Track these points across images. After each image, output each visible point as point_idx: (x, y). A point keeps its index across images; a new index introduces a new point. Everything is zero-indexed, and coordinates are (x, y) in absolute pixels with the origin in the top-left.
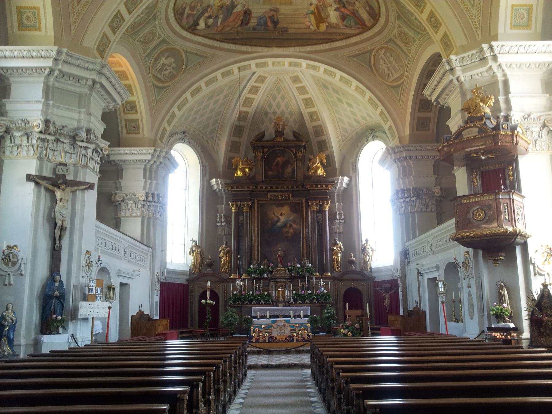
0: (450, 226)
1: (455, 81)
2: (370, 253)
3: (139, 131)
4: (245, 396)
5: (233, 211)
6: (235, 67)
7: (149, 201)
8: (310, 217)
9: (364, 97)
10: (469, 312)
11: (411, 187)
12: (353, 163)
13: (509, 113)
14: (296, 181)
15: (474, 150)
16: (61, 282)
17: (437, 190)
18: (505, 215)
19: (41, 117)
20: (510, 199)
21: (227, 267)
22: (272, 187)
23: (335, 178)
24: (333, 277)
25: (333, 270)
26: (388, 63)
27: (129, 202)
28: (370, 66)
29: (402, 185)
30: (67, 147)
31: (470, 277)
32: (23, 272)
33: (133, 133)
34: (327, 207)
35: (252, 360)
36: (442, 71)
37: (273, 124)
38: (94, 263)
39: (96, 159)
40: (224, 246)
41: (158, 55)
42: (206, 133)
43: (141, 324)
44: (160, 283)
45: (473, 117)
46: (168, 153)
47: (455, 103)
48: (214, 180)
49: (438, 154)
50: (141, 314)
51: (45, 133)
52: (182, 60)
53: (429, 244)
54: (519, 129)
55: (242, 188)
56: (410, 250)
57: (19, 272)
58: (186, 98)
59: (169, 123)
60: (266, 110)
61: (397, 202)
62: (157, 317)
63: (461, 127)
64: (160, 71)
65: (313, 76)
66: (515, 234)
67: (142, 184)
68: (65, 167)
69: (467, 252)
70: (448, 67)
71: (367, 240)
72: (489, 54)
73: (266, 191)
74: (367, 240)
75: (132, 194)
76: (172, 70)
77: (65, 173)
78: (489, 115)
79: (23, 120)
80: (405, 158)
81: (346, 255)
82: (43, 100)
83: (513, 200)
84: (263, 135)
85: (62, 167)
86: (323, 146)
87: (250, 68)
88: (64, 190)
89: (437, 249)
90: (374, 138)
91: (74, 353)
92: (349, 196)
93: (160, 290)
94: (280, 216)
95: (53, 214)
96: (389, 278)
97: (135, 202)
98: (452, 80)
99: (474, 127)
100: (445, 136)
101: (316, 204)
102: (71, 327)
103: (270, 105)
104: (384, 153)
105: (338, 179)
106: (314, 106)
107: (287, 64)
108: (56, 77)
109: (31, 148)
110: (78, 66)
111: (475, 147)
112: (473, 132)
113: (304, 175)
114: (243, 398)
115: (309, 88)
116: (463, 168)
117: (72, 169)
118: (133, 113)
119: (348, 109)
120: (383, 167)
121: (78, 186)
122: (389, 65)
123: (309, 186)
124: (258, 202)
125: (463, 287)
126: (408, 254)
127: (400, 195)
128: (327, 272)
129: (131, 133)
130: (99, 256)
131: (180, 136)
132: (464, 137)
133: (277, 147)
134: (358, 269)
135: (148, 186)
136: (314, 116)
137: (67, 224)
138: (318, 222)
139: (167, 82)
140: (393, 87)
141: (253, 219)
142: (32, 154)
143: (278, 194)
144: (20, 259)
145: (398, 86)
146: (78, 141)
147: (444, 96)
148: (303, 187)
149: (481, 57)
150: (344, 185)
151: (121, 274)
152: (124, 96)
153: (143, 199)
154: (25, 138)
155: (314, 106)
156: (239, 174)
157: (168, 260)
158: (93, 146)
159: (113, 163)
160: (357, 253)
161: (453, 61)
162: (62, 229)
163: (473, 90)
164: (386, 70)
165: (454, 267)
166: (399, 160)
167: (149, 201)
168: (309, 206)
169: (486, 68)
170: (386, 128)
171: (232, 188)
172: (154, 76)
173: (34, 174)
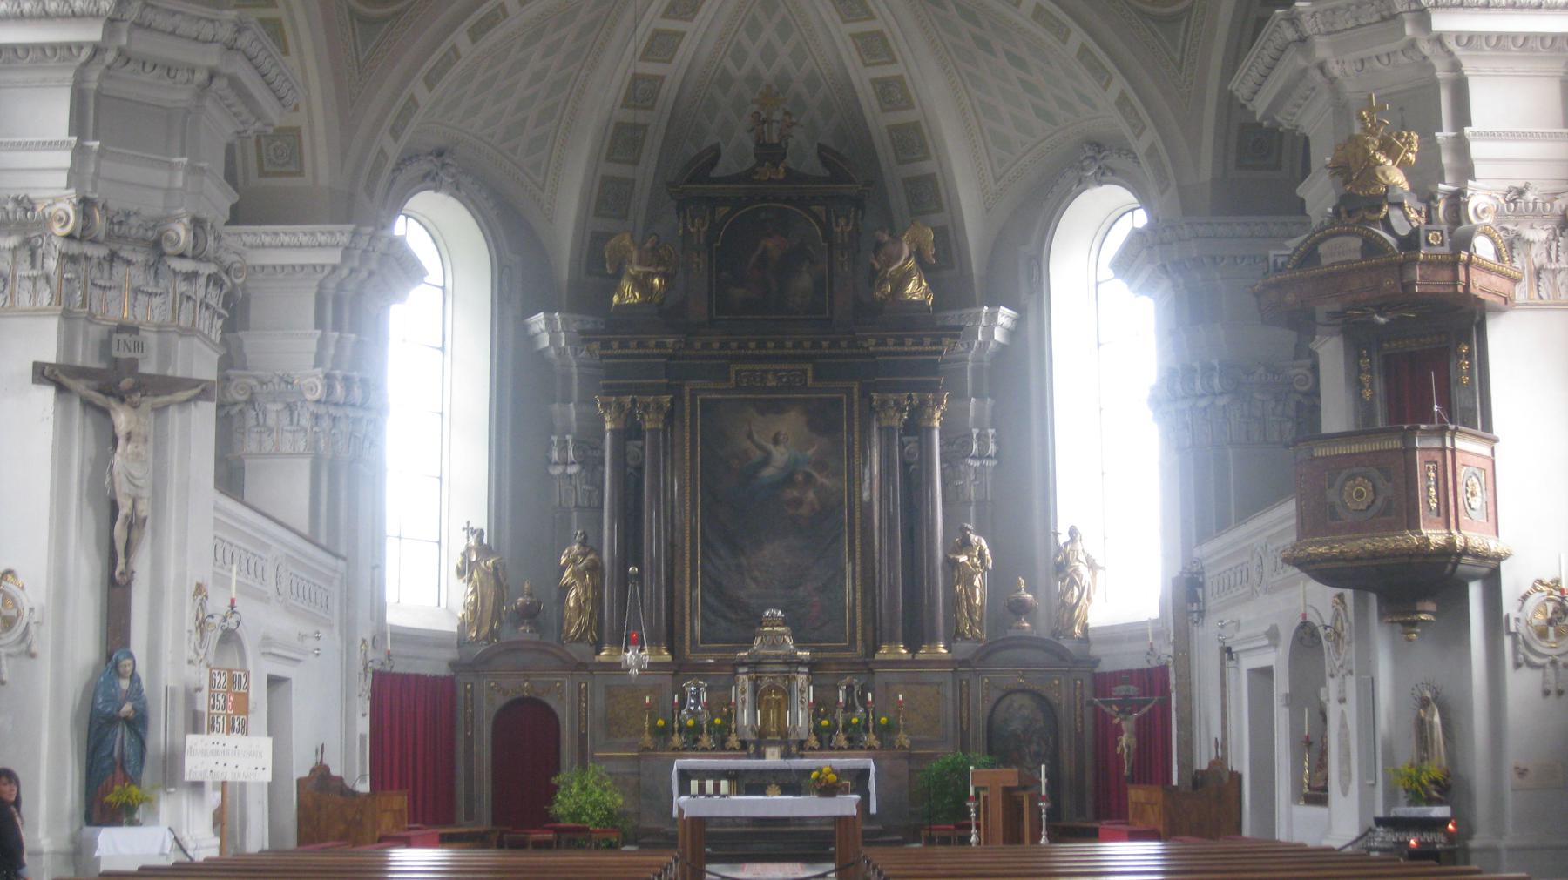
1: (1316, 75)
5: (608, 426)
16: (134, 677)
20: (1444, 449)
23: (966, 311)
24: (953, 661)
25: (954, 635)
27: (273, 407)
30: (137, 276)
32: (34, 649)
33: (281, 174)
34: (938, 415)
39: (213, 303)
40: (576, 547)
44: (370, 676)
48: (541, 315)
50: (321, 774)
51: (81, 239)
53: (1256, 560)
56: (1207, 575)
57: (24, 646)
59: (395, 133)
66: (1449, 553)
67: (312, 345)
70: (1290, 34)
71: (1073, 532)
72: (1406, 7)
74: (1073, 532)
75: (281, 378)
78: (1401, 196)
79: (18, 201)
81: (999, 580)
82: (74, 139)
83: (1453, 451)
84: (715, 154)
85: (124, 336)
86: (927, 195)
88: (135, 406)
90: (1106, 174)
92: (1019, 375)
93: (373, 700)
94: (771, 447)
95: (108, 479)
96: (1138, 663)
97: (290, 408)
101: (897, 403)
102: (165, 807)
105: (978, 317)
106: (894, 61)
108: (108, 67)
109: (41, 284)
110: (173, 33)
117: (151, 339)
121: (170, 393)
123: (872, 341)
124: (693, 396)
126: (1202, 585)
127: (1178, 386)
128: (933, 640)
129: (275, 174)
130: (233, 601)
132: (1324, 261)
134: (1043, 631)
135: (331, 351)
136: (892, 92)
137: (144, 508)
138: (905, 465)
142: (46, 302)
143: (764, 367)
144: (26, 612)
149: (1386, 13)
153: (317, 396)
154: (25, 255)
156: (628, 295)
157: (390, 597)
158: (211, 268)
162: (134, 524)
168: (872, 409)
170: (1140, 147)
171: (605, 345)
173: (53, 361)
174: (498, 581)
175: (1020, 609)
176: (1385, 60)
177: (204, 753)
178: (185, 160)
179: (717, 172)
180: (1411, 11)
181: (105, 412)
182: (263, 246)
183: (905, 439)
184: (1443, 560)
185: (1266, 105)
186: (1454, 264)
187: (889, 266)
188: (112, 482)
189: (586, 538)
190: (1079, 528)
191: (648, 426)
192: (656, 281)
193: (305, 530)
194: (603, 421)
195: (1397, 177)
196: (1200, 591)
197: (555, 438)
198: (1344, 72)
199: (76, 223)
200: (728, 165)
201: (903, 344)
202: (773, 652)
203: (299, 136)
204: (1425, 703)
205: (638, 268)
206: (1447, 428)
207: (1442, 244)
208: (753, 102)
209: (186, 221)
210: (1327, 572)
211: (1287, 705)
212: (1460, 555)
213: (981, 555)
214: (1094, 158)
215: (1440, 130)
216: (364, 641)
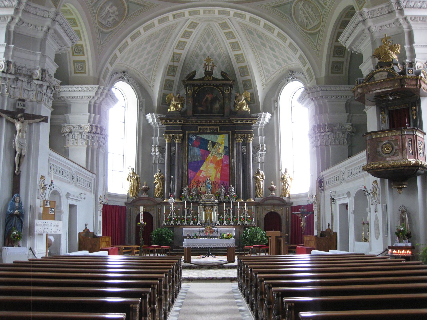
0: (361, 158)
2: (289, 181)
3: (85, 71)
4: (181, 304)
5: (167, 142)
6: (170, 15)
7: (93, 133)
8: (235, 149)
9: (285, 42)
10: (375, 233)
11: (326, 123)
12: (274, 101)
13: (413, 60)
14: (224, 115)
15: (383, 92)
16: (20, 202)
18: (409, 149)
19: (4, 59)
21: (160, 192)
22: (201, 122)
23: (258, 114)
26: (306, 13)
27: (76, 134)
28: (291, 15)
29: (318, 121)
30: (25, 85)
31: (377, 203)
33: (80, 73)
34: (251, 139)
35: (185, 274)
36: (356, 21)
37: (203, 65)
38: (47, 187)
39: (49, 95)
40: (158, 173)
41: (104, 4)
43: (87, 241)
44: (102, 205)
45: (383, 62)
46: (109, 90)
47: (366, 49)
48: (150, 114)
49: (352, 94)
50: (87, 231)
51: (7, 73)
52: (124, 8)
53: (342, 174)
54: (422, 75)
56: (325, 179)
58: (127, 42)
59: (111, 64)
60: (197, 53)
62: (100, 235)
63: (373, 71)
64: (104, 19)
65: (240, 23)
68: (23, 103)
69: (375, 181)
70: (361, 19)
71: (286, 170)
72: (396, 8)
73: (196, 125)
74: (286, 170)
75: (79, 126)
76: (115, 18)
80: (321, 97)
81: (267, 182)
82: (6, 44)
86: (248, 85)
87: (184, 16)
89: (349, 178)
90: (294, 79)
91: (33, 264)
92: (272, 131)
95: (13, 144)
96: (306, 203)
97: (81, 134)
98: (364, 30)
99: (384, 71)
100: (359, 78)
104: (303, 93)
105: (261, 115)
106: (240, 50)
107: (216, 12)
108: (17, 24)
111: (385, 88)
112: (382, 76)
113: (231, 110)
114: (180, 306)
115: (236, 34)
116: (373, 107)
118: (81, 55)
119: (271, 52)
122: (308, 15)
123: (235, 121)
125: (370, 212)
126: (323, 182)
127: (316, 130)
128: (250, 197)
129: (78, 73)
130: (52, 181)
131: (120, 75)
132: (376, 80)
133: (207, 85)
134: (278, 195)
136: (240, 58)
138: (243, 153)
139: (111, 28)
140: (311, 34)
141: (184, 150)
145: (315, 34)
146: (35, 79)
147: (357, 43)
149: (390, 11)
150: (267, 120)
151: (70, 197)
152: (74, 40)
153: (88, 131)
156: (172, 109)
158: (48, 84)
159: (62, 99)
160: (277, 181)
161: (366, 13)
163: (383, 39)
164: (305, 20)
165: (364, 194)
166: (316, 99)
167: (93, 133)
168: (234, 138)
169: (393, 20)
172: (100, 23)
174: (138, 182)
175: (272, 189)
176: (388, 26)
177: (41, 225)
178: (40, 52)
179: (194, 78)
180: (398, 9)
181: (13, 124)
182: (74, 91)
183: (243, 147)
185: (350, 43)
186: (417, 79)
187: (239, 102)
188: (15, 144)
189: (160, 171)
190: (287, 169)
191: (177, 142)
192: (179, 105)
193: (85, 166)
194: (165, 141)
195: (395, 57)
196: (322, 184)
197: (153, 146)
198: (376, 30)
199: (5, 68)
200: (197, 77)
201: (242, 121)
202: (208, 200)
203: (85, 63)
204: (403, 212)
205: (174, 102)
206: (415, 129)
207: (413, 73)
208: (204, 60)
209: (39, 69)
210: (375, 172)
211: (353, 213)
212: (419, 167)
213: (262, 176)
214: (291, 75)
215: (405, 45)
216: (100, 196)
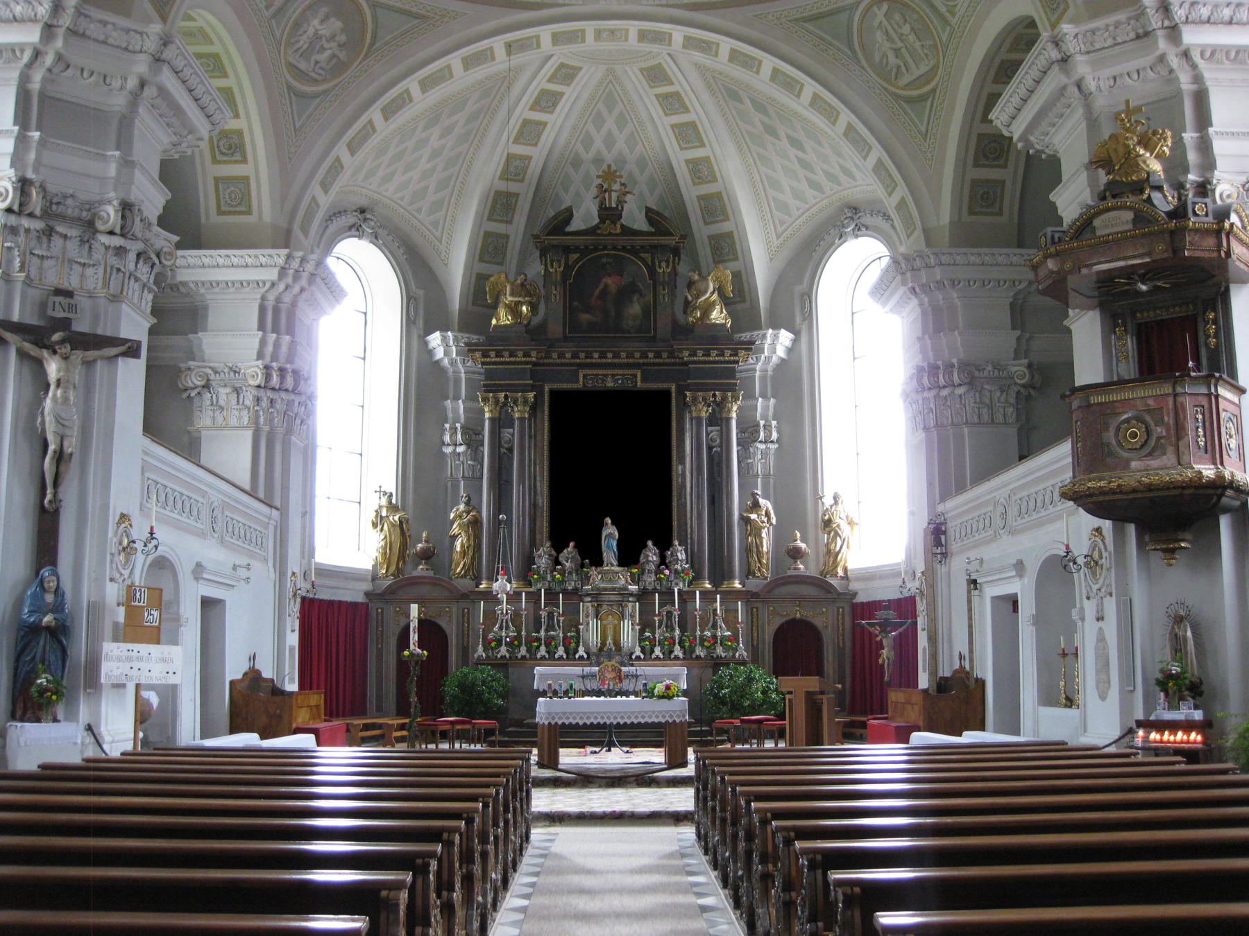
0: (1057, 461)
2: (845, 530)
3: (250, 207)
5: (487, 415)
6: (498, 44)
7: (273, 389)
8: (688, 435)
9: (834, 124)
10: (1098, 682)
11: (954, 361)
12: (802, 295)
13: (1208, 176)
14: (654, 338)
16: (58, 591)
17: (1018, 368)
18: (1196, 434)
19: (11, 172)
21: (469, 562)
22: (589, 356)
23: (756, 333)
27: (223, 391)
28: (850, 45)
29: (931, 354)
30: (73, 248)
33: (235, 213)
34: (735, 408)
35: (542, 800)
36: (1041, 63)
37: (594, 191)
38: (139, 546)
39: (144, 278)
40: (462, 507)
41: (304, 11)
42: (402, 199)
43: (254, 704)
44: (299, 600)
45: (1120, 181)
46: (320, 263)
47: (1070, 144)
48: (438, 334)
49: (1031, 276)
50: (253, 676)
51: (20, 213)
52: (364, 23)
53: (1000, 509)
54: (1234, 218)
55: (511, 356)
56: (949, 525)
58: (370, 122)
59: (325, 187)
60: (577, 154)
61: (920, 397)
62: (292, 686)
64: (306, 55)
65: (701, 69)
68: (68, 300)
69: (1098, 530)
70: (1055, 55)
71: (836, 498)
72: (1160, 23)
73: (573, 365)
74: (836, 498)
75: (231, 369)
77: (70, 316)
80: (940, 285)
81: (781, 534)
82: (17, 128)
86: (726, 248)
87: (538, 46)
90: (859, 230)
91: (96, 773)
92: (795, 384)
95: (39, 420)
97: (237, 391)
98: (1064, 88)
99: (1123, 207)
100: (1049, 229)
103: (588, 142)
104: (886, 272)
105: (764, 336)
106: (703, 145)
107: (633, 35)
108: (49, 70)
111: (1125, 258)
112: (1118, 221)
113: (675, 323)
115: (690, 99)
116: (1091, 313)
118: (236, 162)
119: (793, 152)
120: (884, 305)
122: (900, 44)
123: (686, 353)
125: (1083, 619)
126: (944, 533)
127: (925, 381)
128: (731, 577)
129: (230, 213)
130: (152, 528)
131: (351, 219)
132: (1099, 233)
133: (605, 248)
134: (813, 571)
136: (702, 170)
138: (710, 448)
139: (324, 81)
140: (910, 100)
141: (539, 438)
143: (605, 372)
145: (923, 98)
148: (671, 355)
149: (1141, 31)
150: (781, 352)
151: (205, 576)
152: (217, 117)
153: (257, 383)
155: (703, 145)
156: (503, 318)
158: (139, 246)
159: (182, 289)
161: (1069, 38)
163: (1119, 114)
165: (1065, 567)
166: (926, 288)
167: (273, 389)
168: (685, 404)
169: (1150, 59)
172: (293, 67)
174: (403, 533)
175: (796, 554)
176: (1135, 77)
177: (119, 659)
178: (117, 153)
179: (568, 229)
180: (1163, 28)
181: (39, 364)
183: (710, 429)
184: (1211, 492)
185: (1023, 127)
186: (1218, 232)
187: (698, 297)
188: (43, 422)
189: (469, 500)
190: (840, 493)
191: (517, 415)
192: (524, 308)
193: (247, 487)
194: (483, 412)
195: (1156, 166)
196: (943, 537)
197: (447, 426)
198: (1099, 89)
200: (576, 225)
201: (709, 355)
202: (610, 586)
204: (1179, 620)
205: (510, 299)
207: (1207, 215)
208: (598, 177)
209: (115, 203)
210: (1096, 503)
212: (1225, 488)
213: (767, 515)
214: (852, 219)
215: (1185, 131)
216: (294, 574)
